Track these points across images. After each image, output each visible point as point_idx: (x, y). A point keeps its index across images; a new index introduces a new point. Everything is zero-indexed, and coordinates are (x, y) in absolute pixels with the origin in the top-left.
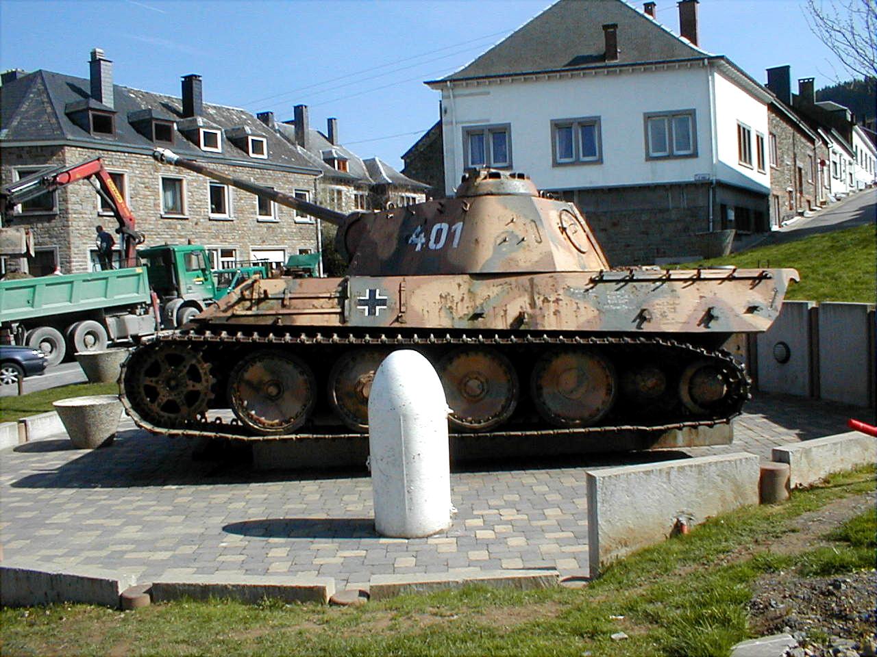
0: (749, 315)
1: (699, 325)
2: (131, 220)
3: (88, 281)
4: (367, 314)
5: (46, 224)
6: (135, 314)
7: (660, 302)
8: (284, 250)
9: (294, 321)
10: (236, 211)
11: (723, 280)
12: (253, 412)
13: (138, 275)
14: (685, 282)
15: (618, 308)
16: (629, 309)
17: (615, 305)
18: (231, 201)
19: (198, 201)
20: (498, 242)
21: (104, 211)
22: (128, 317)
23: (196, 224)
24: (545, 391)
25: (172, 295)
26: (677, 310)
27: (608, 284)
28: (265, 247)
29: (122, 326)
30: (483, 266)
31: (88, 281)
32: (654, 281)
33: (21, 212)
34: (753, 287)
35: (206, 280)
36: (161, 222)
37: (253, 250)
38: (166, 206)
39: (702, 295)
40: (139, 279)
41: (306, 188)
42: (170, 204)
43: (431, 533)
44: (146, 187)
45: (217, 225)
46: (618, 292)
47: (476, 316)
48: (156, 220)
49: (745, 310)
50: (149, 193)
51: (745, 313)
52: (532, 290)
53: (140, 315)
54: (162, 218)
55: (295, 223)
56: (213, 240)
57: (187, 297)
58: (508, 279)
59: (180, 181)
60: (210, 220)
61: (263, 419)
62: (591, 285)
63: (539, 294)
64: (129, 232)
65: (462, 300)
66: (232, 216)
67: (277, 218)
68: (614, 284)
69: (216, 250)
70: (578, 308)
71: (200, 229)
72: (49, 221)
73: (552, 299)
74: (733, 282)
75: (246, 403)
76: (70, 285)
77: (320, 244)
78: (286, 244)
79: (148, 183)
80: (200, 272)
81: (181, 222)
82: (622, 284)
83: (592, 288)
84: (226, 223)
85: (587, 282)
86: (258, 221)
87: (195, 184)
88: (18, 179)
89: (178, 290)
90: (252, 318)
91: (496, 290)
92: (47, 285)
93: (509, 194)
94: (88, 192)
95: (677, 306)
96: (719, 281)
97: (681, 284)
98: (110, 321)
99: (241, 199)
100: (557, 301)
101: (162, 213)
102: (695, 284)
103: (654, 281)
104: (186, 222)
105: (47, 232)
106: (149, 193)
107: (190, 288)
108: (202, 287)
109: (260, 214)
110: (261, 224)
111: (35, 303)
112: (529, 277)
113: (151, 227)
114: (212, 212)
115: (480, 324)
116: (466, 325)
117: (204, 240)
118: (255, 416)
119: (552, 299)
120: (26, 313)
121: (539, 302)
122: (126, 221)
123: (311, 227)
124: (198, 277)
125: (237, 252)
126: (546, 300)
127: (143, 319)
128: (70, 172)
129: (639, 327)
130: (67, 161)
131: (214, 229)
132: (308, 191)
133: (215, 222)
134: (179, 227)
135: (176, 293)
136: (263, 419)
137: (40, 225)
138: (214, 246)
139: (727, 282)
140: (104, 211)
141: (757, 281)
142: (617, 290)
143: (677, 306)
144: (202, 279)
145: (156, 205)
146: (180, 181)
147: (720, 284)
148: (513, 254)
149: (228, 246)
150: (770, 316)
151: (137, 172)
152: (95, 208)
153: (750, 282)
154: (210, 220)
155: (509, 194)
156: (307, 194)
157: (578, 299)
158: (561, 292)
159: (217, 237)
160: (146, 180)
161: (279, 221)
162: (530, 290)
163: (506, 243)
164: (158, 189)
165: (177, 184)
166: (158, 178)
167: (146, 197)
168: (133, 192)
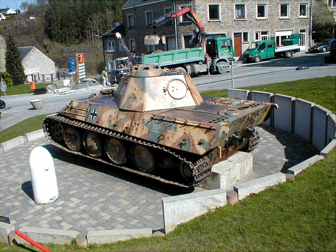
0: (198, 146)
1: (178, 146)
2: (203, 28)
3: (179, 53)
4: (96, 117)
5: (189, 26)
6: (199, 64)
7: (169, 133)
8: (292, 31)
9: (76, 117)
10: (269, 15)
11: (196, 127)
12: (70, 143)
13: (200, 50)
14: (182, 125)
15: (155, 131)
16: (158, 133)
17: (155, 130)
18: (267, 11)
19: (251, 13)
20: (129, 97)
21: (210, 20)
22: (196, 66)
23: (250, 22)
24: (136, 157)
25: (216, 57)
26: (174, 137)
27: (156, 120)
28: (283, 30)
29: (193, 69)
30: (123, 105)
31: (179, 53)
32: (171, 122)
33: (182, 21)
34: (206, 132)
35: (230, 51)
36: (234, 22)
37: (277, 31)
38: (236, 17)
39: (185, 132)
40: (200, 52)
41: (306, 2)
42: (240, 14)
43: (40, 203)
44: (228, 9)
45: (260, 22)
46: (158, 125)
47: (115, 126)
48: (232, 22)
49: (198, 143)
50: (230, 11)
51: (197, 144)
52: (133, 118)
53: (201, 65)
54: (234, 21)
55: (299, 19)
56: (258, 28)
57: (221, 58)
58: (128, 113)
59: (244, 5)
60: (256, 20)
61: (72, 145)
62: (151, 120)
63: (135, 120)
64: (201, 33)
65: (114, 118)
66: (267, 18)
67: (290, 17)
68: (158, 121)
69: (259, 32)
70: (143, 129)
71: (251, 24)
72: (190, 25)
73: (137, 123)
74: (199, 129)
75: (68, 140)
76: (172, 55)
77: (311, 27)
78: (293, 28)
79: (229, 7)
80: (228, 48)
81: (243, 22)
82: (160, 121)
83: (150, 121)
84: (264, 21)
85: (150, 118)
86: (280, 19)
87: (250, 6)
88: (181, 9)
89: (218, 55)
90: (68, 114)
91: (124, 116)
92: (164, 55)
93: (138, 77)
94: (204, 13)
95: (174, 135)
96: (194, 127)
97: (180, 126)
98: (188, 67)
99: (272, 10)
100: (139, 124)
101: (235, 19)
102: (185, 127)
103: (171, 122)
104: (246, 21)
105: (190, 29)
106: (230, 11)
107: (223, 54)
108: (229, 54)
109: (281, 16)
110: (281, 20)
111: (159, 62)
112: (134, 113)
113: (230, 25)
114: (258, 17)
115: (115, 129)
116: (111, 128)
117: (253, 28)
118: (70, 144)
119: (137, 123)
120: (170, 63)
121: (133, 124)
122: (201, 29)
123: (307, 20)
124: (226, 50)
125: (269, 32)
126: (135, 123)
127: (202, 66)
128: (177, 14)
129: (158, 141)
130: (196, 3)
131: (258, 24)
132: (307, 4)
133: (259, 21)
134: (242, 24)
135: (217, 56)
136: (72, 145)
137: (187, 26)
138: (258, 31)
139: (197, 129)
140: (210, 20)
141: (209, 130)
142: (158, 124)
143: (174, 135)
144: (228, 50)
145: (233, 16)
146: (244, 5)
147: (194, 128)
148: (132, 103)
149: (264, 30)
150: (206, 148)
151: (225, 4)
152: (207, 19)
153: (205, 130)
154: (256, 20)
155: (138, 77)
156: (307, 5)
157: (145, 125)
158: (141, 121)
159: (259, 27)
160: (228, 6)
161: (290, 18)
162: (132, 118)
163: (131, 98)
164: (234, 9)
165: (243, 6)
166: (233, 5)
167: (228, 13)
168: (222, 12)
